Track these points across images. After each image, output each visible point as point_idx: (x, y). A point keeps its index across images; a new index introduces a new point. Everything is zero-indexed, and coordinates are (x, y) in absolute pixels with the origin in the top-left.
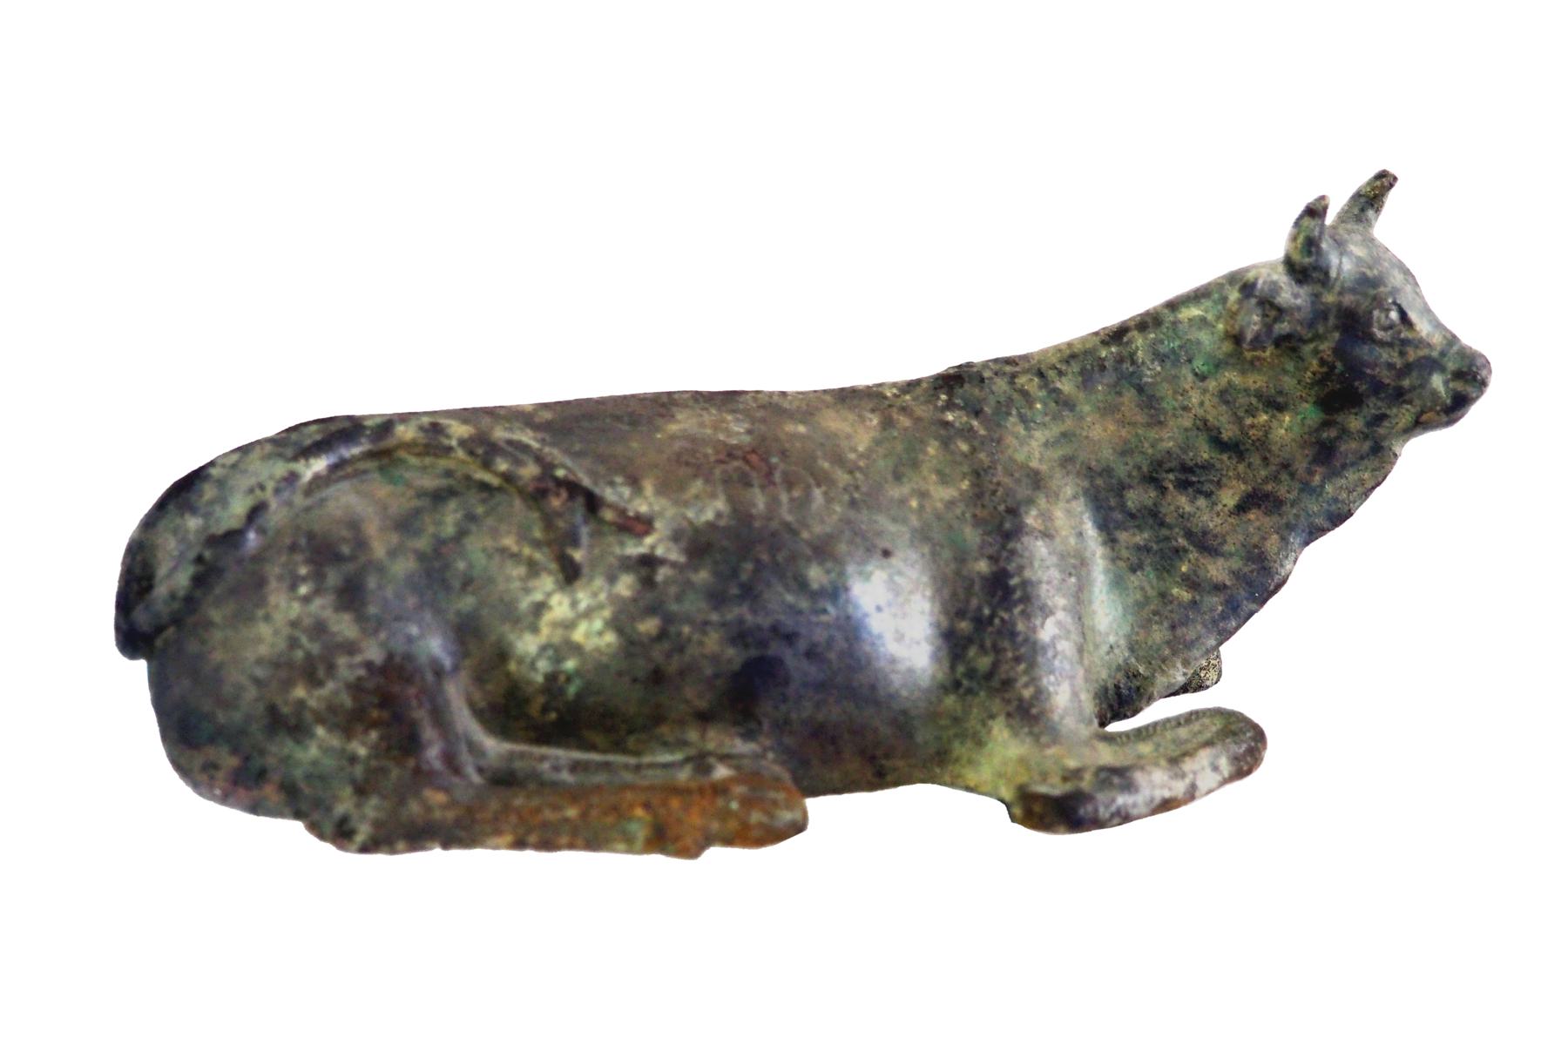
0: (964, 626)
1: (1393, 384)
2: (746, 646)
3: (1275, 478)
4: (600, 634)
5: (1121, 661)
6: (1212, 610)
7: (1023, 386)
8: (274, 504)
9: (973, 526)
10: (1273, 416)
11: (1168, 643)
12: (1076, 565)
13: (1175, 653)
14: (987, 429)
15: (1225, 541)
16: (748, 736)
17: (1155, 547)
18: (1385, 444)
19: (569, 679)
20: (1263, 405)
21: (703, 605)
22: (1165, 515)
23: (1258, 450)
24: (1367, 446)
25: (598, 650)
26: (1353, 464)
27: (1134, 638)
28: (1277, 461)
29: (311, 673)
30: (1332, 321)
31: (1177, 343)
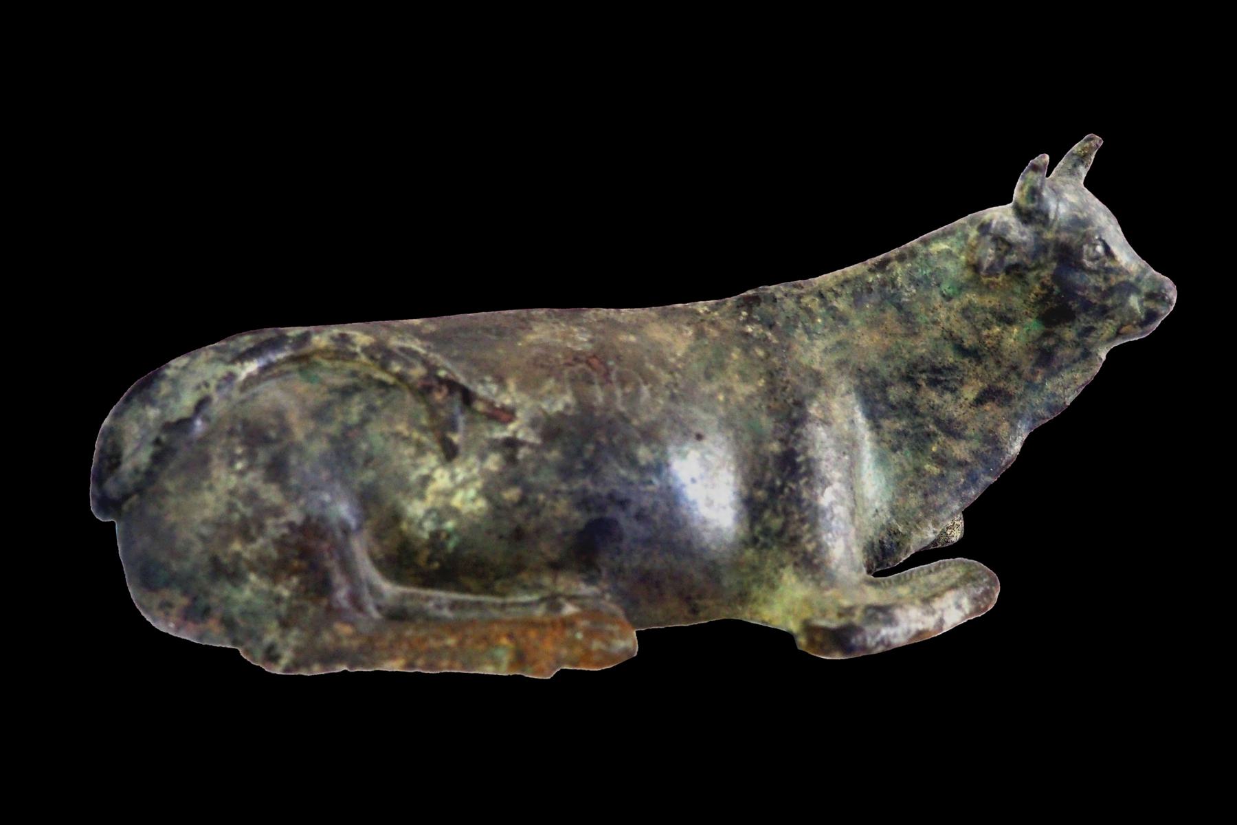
0: (761, 494)
1: (1099, 303)
2: (589, 510)
3: (1006, 377)
4: (473, 500)
5: (884, 522)
6: (956, 482)
7: (807, 305)
8: (216, 398)
9: (768, 415)
10: (1005, 329)
11: (922, 507)
12: (849, 446)
13: (927, 515)
14: (778, 338)
15: (967, 427)
16: (590, 581)
17: (911, 432)
18: (1093, 350)
19: (449, 536)
20: (997, 319)
21: (555, 478)
22: (919, 407)
23: (992, 355)
24: (1078, 352)
25: (471, 513)
26: (1067, 367)
27: (895, 503)
28: (1008, 364)
29: (246, 531)
30: (1051, 253)
31: (929, 271)
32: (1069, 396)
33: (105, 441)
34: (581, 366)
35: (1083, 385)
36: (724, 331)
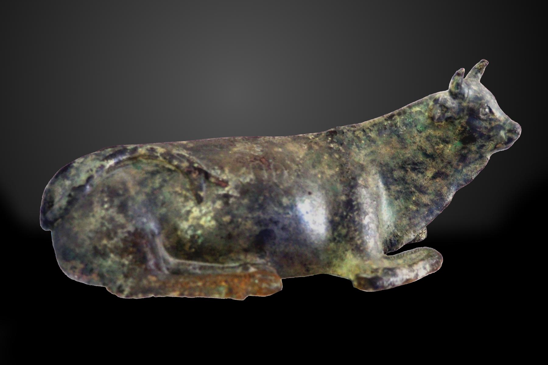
0: (337, 219)
1: (487, 134)
2: (261, 226)
3: (446, 167)
4: (210, 221)
5: (392, 231)
6: (424, 213)
7: (357, 135)
8: (96, 176)
10: (445, 145)
11: (408, 224)
12: (376, 197)
13: (410, 228)
14: (345, 150)
15: (428, 189)
16: (262, 257)
17: (404, 191)
18: (484, 155)
19: (199, 237)
20: (442, 141)
21: (246, 211)
22: (407, 180)
23: (440, 157)
24: (478, 156)
25: (209, 227)
26: (473, 162)
27: (396, 223)
28: (446, 161)
29: (109, 235)
30: (465, 112)
31: (411, 120)
32: (473, 175)
33: (47, 195)
34: (257, 162)
35: (480, 170)
36: (321, 147)
